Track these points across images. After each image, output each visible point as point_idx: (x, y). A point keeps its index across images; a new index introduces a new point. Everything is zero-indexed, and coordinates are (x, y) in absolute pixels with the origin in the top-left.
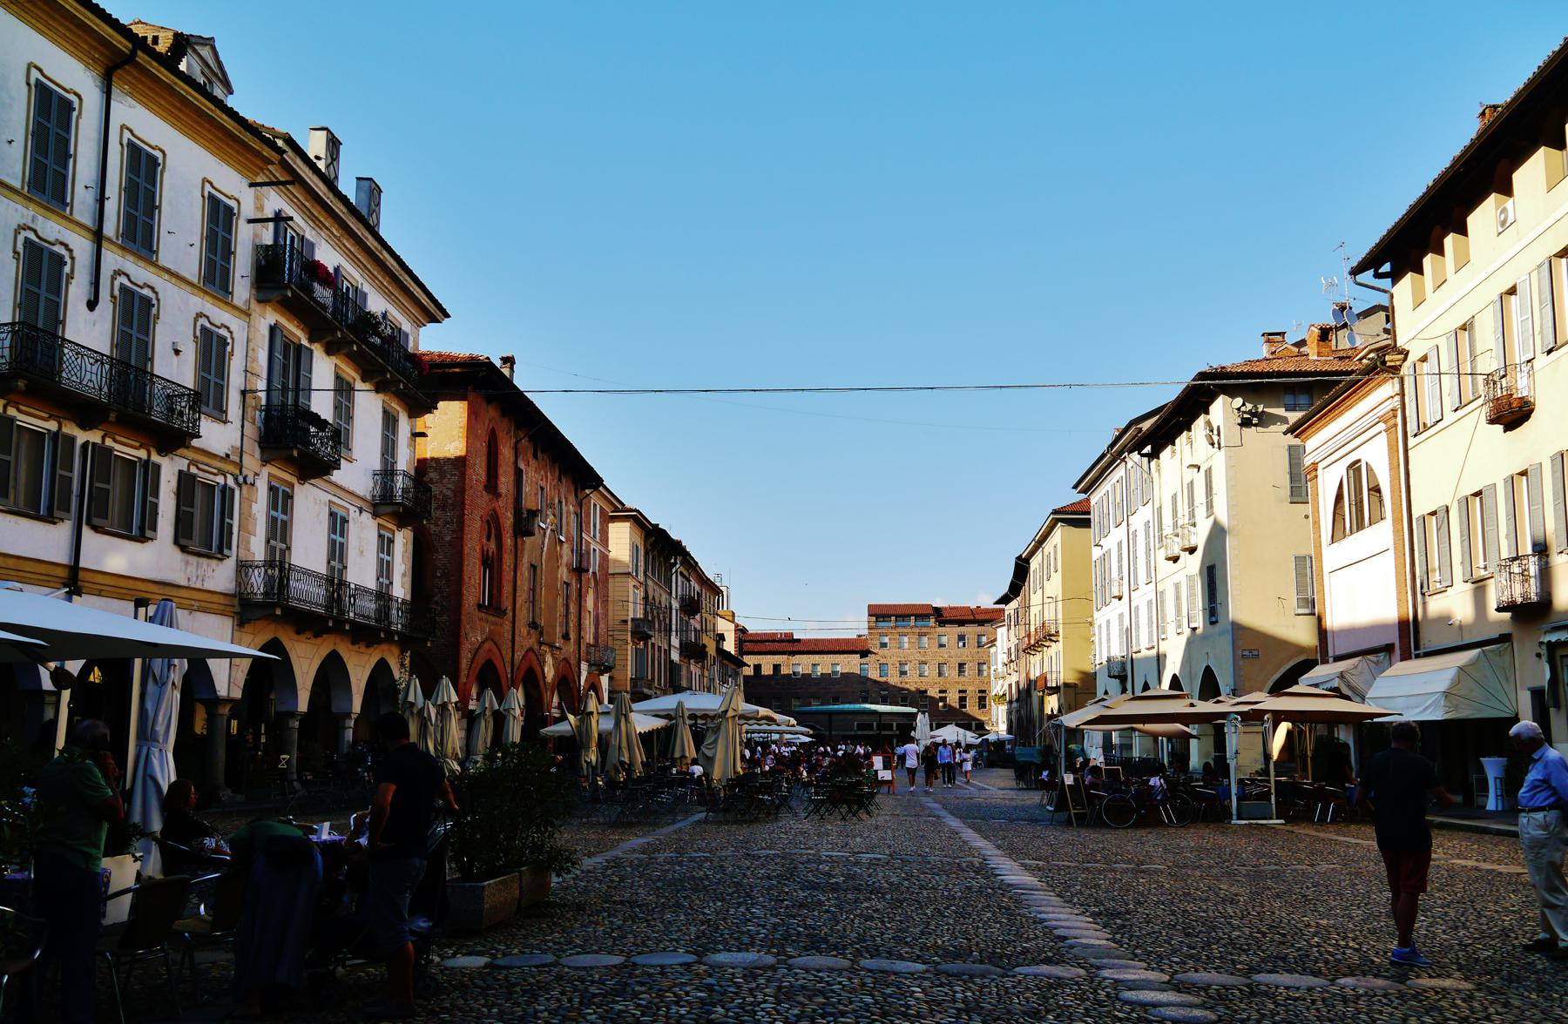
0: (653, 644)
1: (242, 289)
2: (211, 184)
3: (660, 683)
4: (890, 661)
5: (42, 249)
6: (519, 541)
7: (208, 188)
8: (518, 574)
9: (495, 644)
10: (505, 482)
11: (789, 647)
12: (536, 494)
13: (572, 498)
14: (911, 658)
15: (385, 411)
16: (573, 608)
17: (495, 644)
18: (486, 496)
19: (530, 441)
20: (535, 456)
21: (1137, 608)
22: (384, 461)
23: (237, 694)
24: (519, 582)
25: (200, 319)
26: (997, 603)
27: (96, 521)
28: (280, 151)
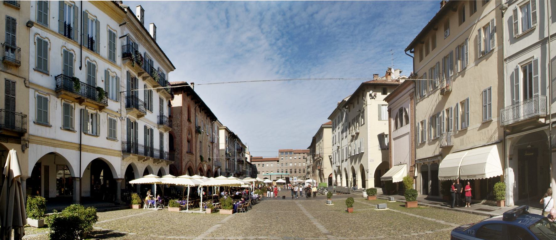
0: (231, 160)
1: (119, 59)
2: (109, 26)
3: (232, 170)
4: (283, 163)
5: (91, 63)
6: (197, 135)
7: (108, 28)
8: (197, 144)
9: (191, 162)
10: (192, 119)
11: (262, 160)
12: (201, 122)
13: (210, 123)
14: (288, 162)
15: (160, 98)
16: (211, 152)
17: (191, 162)
18: (188, 123)
19: (199, 107)
20: (200, 112)
21: (343, 149)
22: (160, 113)
23: (123, 177)
24: (197, 146)
25: (87, 59)
26: (308, 148)
27: (85, 132)
28: (126, 12)
